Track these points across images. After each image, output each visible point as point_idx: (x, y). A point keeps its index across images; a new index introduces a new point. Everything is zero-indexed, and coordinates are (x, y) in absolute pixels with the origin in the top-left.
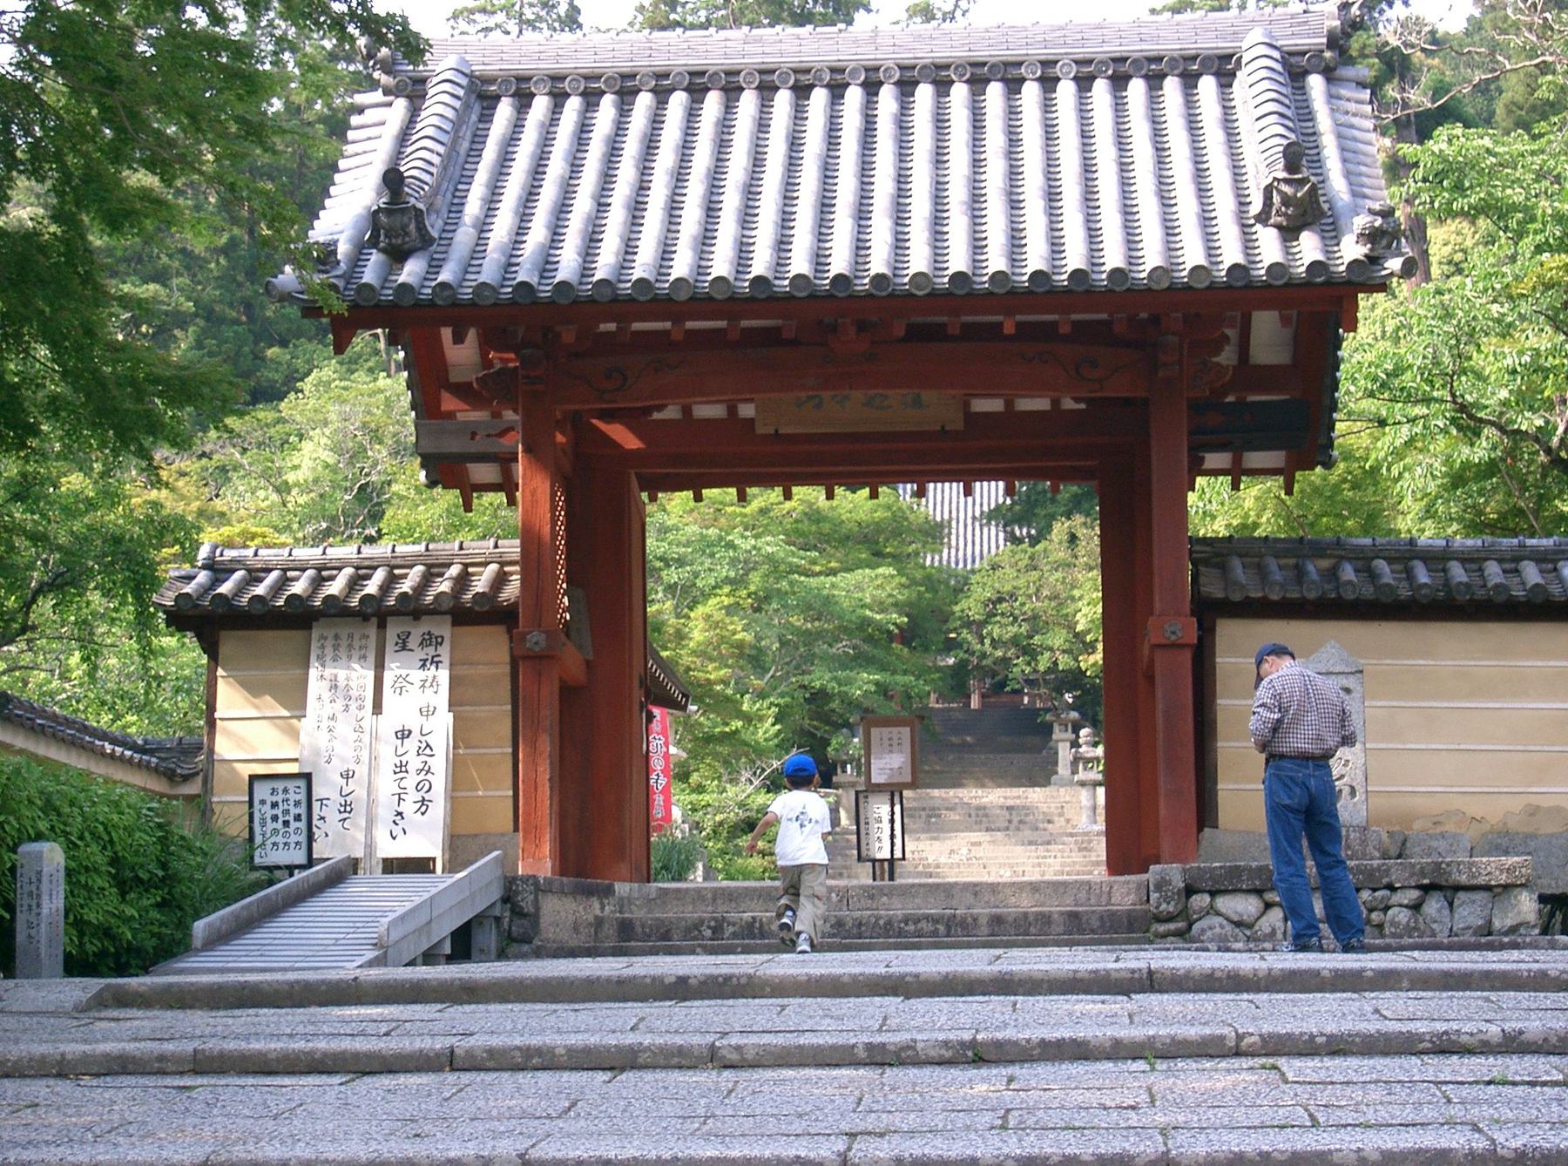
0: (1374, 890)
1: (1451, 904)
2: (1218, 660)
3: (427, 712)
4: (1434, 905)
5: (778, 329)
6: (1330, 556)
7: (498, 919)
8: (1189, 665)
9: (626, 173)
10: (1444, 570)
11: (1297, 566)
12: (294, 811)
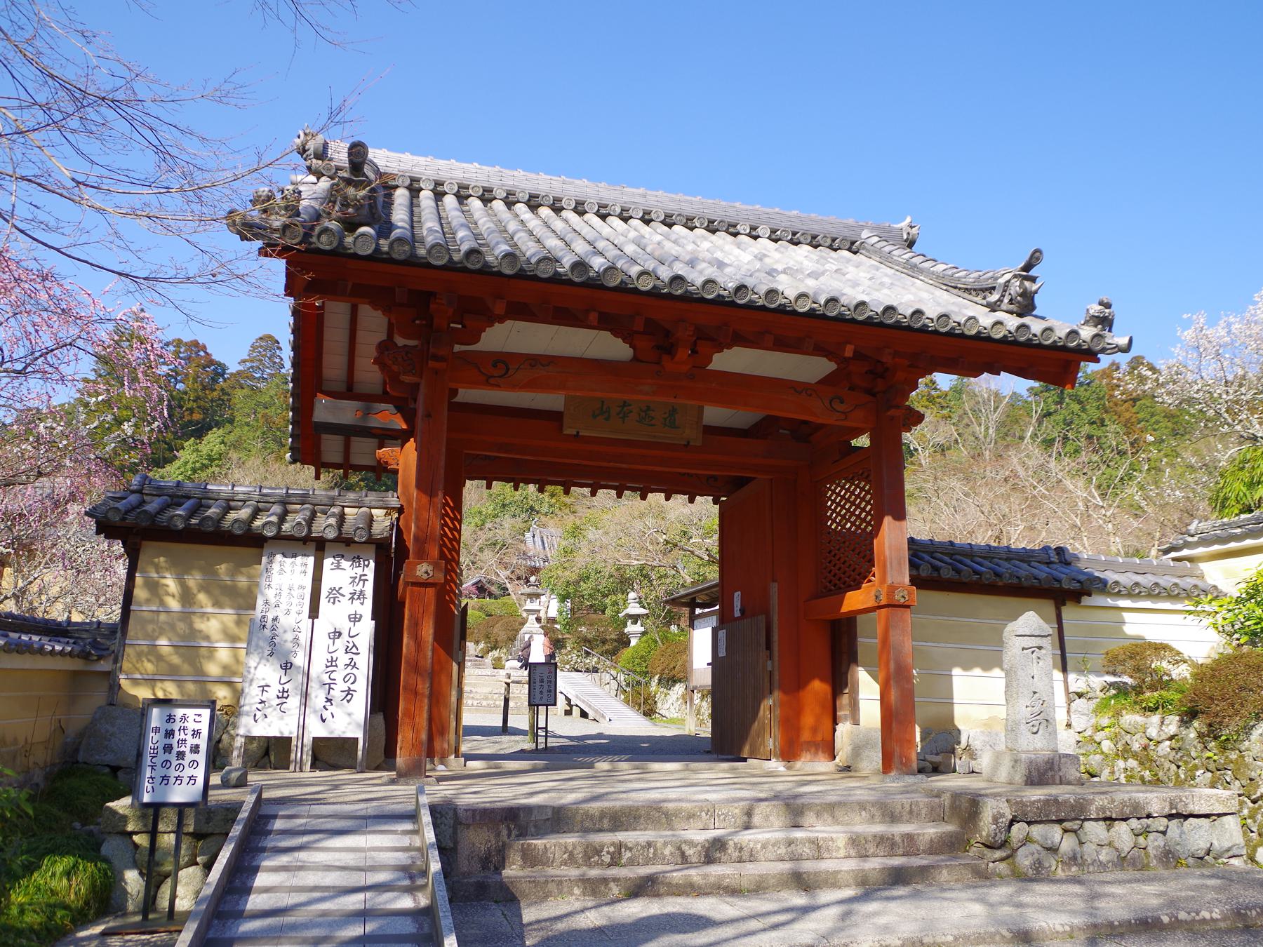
3: (355, 618)
12: (191, 741)
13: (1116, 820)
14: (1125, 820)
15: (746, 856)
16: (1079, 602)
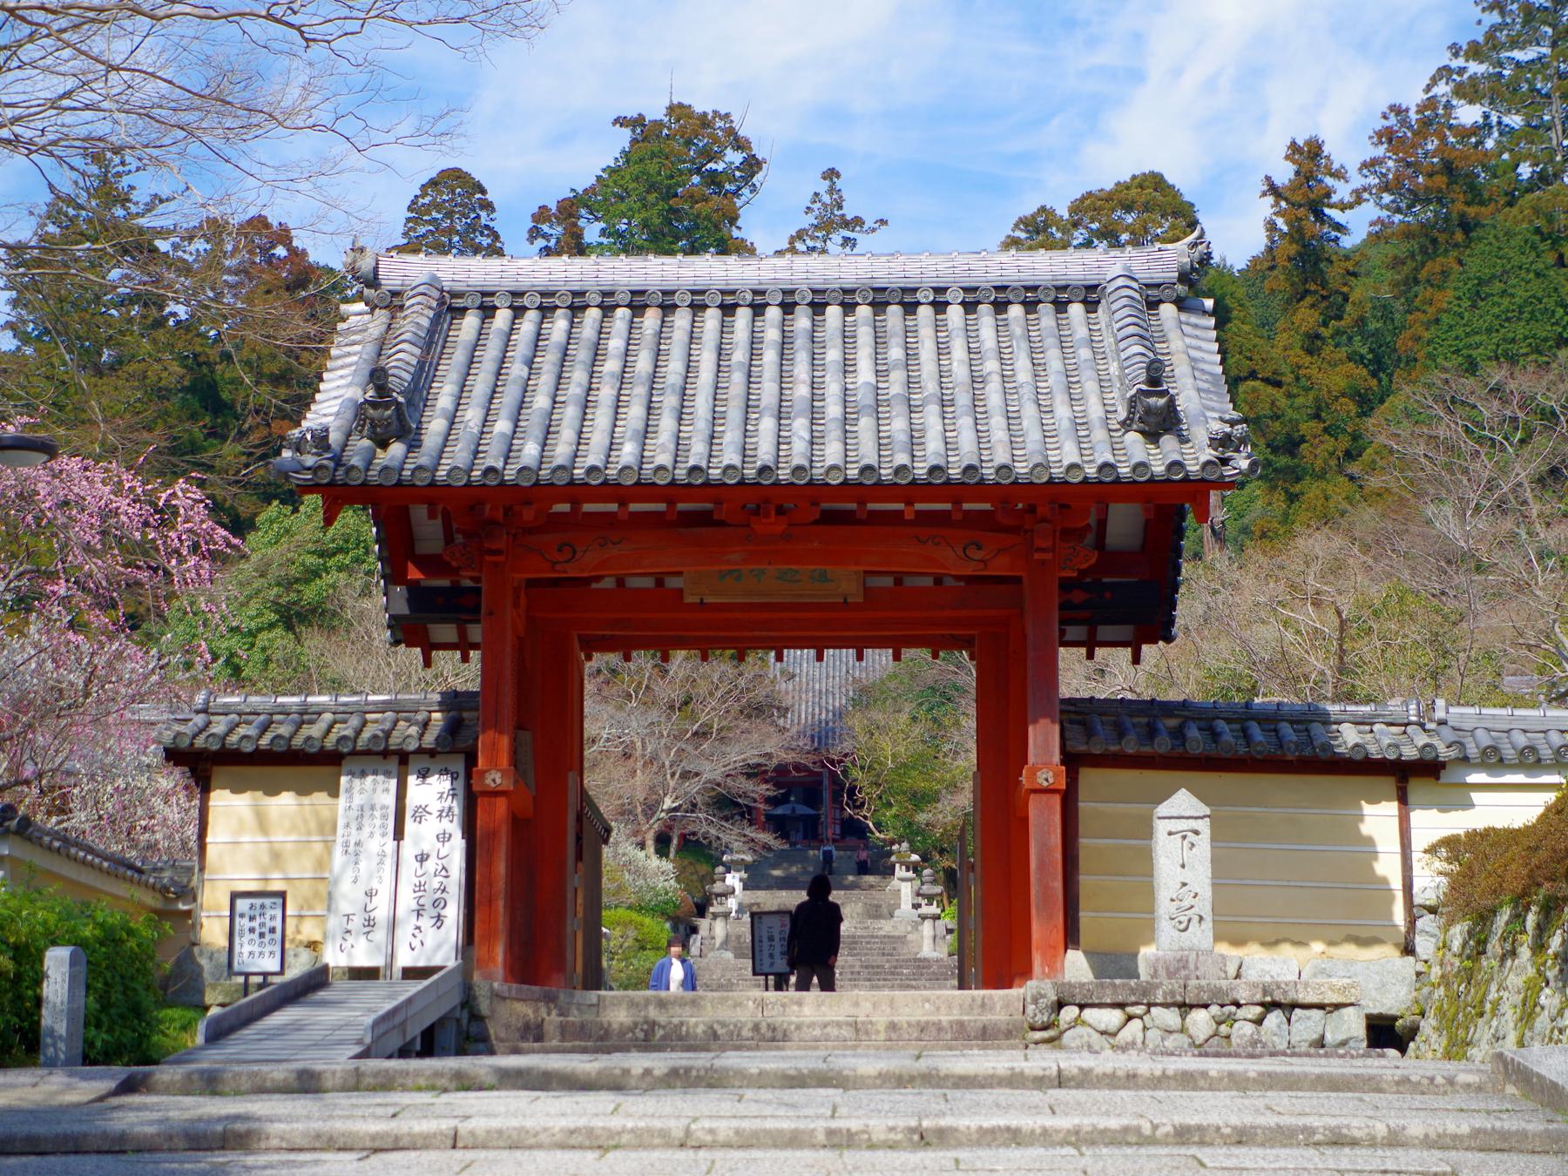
0: (1222, 1006)
1: (1289, 1020)
2: (1081, 805)
4: (1274, 1019)
5: (710, 512)
6: (1176, 716)
7: (458, 1020)
8: (1058, 808)
9: (578, 376)
10: (1275, 730)
11: (1148, 724)
12: (269, 924)
13: (1192, 1007)
14: (1206, 1006)
15: (779, 1035)
16: (1438, 778)
